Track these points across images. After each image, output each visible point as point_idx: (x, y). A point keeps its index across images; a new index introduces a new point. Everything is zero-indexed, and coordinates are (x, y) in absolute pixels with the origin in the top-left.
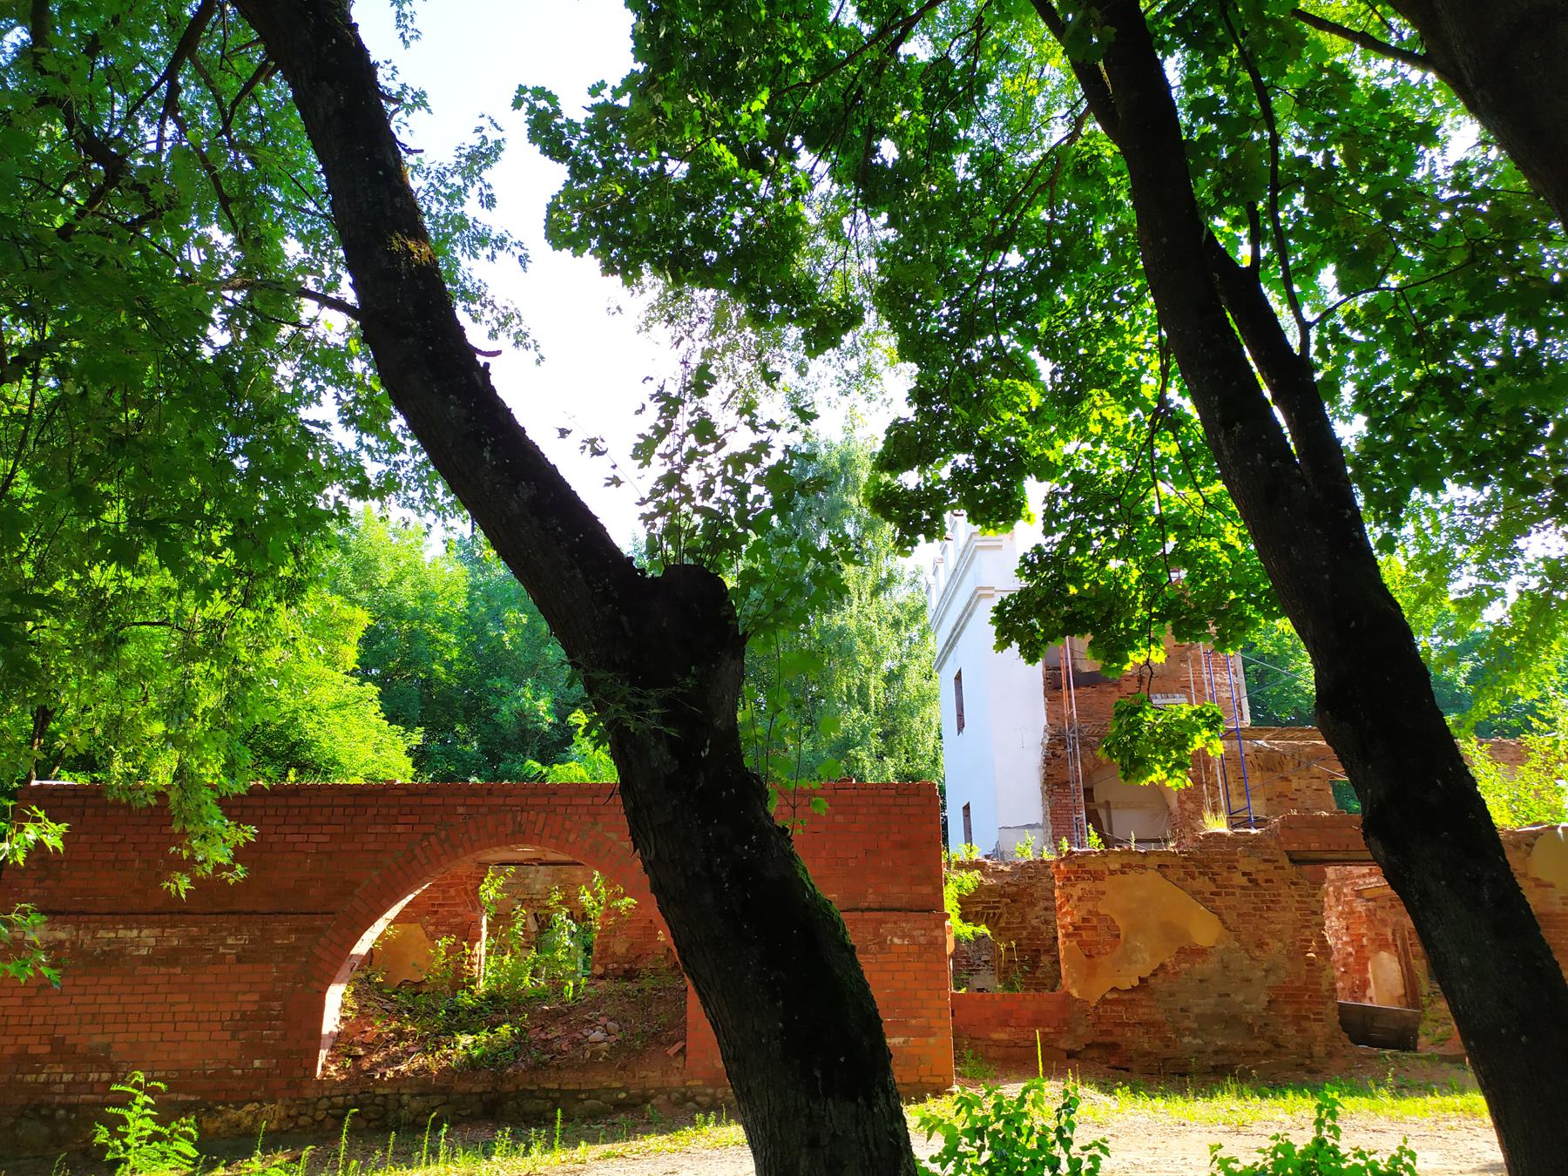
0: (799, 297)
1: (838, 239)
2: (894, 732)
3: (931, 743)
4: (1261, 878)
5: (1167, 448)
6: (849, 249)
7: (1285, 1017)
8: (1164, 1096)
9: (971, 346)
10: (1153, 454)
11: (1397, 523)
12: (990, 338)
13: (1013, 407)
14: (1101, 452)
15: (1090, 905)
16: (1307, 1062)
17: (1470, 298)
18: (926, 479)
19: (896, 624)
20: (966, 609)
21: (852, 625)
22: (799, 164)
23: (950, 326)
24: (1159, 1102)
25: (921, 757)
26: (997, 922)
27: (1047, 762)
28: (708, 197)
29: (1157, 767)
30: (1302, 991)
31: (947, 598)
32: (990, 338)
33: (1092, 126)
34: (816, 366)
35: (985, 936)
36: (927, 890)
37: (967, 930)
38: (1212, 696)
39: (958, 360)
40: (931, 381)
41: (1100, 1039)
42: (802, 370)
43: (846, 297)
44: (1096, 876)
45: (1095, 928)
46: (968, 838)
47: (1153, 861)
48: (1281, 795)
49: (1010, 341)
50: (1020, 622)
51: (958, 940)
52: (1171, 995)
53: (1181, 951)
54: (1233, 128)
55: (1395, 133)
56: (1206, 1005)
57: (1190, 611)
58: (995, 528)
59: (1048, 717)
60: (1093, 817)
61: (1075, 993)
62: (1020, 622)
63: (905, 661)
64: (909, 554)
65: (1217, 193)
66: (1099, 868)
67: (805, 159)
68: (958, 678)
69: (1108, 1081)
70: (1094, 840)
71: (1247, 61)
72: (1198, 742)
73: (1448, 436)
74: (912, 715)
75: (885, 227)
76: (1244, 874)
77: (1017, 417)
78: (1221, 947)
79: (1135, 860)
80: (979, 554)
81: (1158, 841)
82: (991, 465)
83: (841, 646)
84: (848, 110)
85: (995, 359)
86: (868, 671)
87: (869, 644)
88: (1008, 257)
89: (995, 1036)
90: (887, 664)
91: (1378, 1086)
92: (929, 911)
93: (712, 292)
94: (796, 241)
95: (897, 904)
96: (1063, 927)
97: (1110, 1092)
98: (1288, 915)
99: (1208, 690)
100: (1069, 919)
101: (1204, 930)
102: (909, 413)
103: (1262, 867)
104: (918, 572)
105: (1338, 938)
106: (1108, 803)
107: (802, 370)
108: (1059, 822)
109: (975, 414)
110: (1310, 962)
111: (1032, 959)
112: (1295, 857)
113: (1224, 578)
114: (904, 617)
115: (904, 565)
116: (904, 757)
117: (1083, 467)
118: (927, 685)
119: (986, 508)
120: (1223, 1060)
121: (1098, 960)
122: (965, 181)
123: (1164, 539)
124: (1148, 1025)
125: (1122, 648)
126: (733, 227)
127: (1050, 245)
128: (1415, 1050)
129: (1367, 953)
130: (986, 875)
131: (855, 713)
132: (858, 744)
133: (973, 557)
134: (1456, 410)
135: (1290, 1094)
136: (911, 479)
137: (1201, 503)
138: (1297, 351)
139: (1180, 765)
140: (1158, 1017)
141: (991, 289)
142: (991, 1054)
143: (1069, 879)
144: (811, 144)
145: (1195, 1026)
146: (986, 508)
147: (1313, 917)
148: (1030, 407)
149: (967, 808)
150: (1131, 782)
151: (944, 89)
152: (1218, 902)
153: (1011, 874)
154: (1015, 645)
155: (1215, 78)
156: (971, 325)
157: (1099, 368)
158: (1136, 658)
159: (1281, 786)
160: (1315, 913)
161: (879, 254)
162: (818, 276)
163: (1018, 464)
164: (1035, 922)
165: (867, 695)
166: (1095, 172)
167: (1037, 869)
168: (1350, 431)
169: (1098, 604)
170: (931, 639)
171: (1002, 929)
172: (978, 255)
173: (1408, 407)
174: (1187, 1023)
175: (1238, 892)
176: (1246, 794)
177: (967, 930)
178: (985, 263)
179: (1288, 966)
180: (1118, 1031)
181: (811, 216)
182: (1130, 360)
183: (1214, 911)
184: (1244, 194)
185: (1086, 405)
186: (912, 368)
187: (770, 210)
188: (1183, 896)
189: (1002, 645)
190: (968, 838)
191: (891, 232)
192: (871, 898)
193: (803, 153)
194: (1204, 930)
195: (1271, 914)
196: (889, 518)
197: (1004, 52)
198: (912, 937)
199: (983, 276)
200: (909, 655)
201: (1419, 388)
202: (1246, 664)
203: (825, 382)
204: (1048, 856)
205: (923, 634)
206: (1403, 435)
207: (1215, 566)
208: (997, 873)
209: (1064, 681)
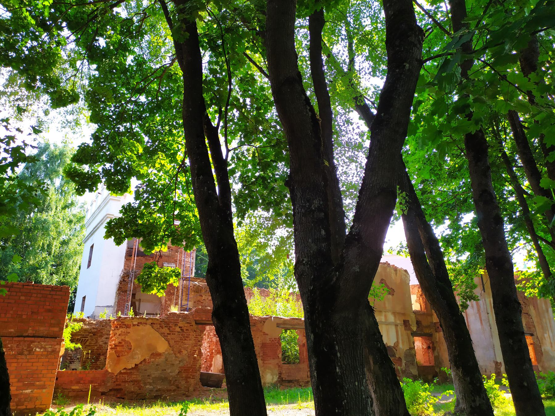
0: (52, 84)
1: (73, 68)
2: (60, 264)
3: (75, 270)
4: (185, 329)
5: (182, 178)
6: (81, 74)
7: (182, 377)
8: (134, 408)
9: (120, 124)
10: (177, 180)
11: (243, 218)
12: (128, 124)
13: (132, 151)
14: (160, 175)
15: (123, 337)
16: (187, 393)
17: (275, 156)
18: (92, 170)
19: (70, 222)
20: (101, 221)
21: (51, 219)
22: (62, 33)
23: (114, 115)
24: (132, 410)
25: (70, 276)
26: (86, 343)
27: (121, 282)
28: (16, 32)
29: (155, 288)
30: (190, 368)
31: (94, 216)
32: (128, 124)
33: (176, 63)
34: (54, 113)
35: (80, 348)
36: (56, 329)
37: (72, 346)
38: (184, 265)
39: (114, 128)
40: (102, 134)
41: (116, 387)
42: (46, 113)
43: (72, 90)
44: (128, 327)
45: (123, 346)
46: (82, 310)
47: (150, 322)
48: (199, 301)
49: (136, 127)
50: (116, 230)
51: (67, 350)
52: (145, 370)
53: (153, 354)
54: (220, 82)
55: (264, 100)
56: (156, 374)
57: (178, 236)
58: (116, 193)
59: (125, 266)
60: (133, 304)
61: (110, 370)
62: (116, 230)
63: (71, 237)
64: (81, 195)
65: (211, 100)
66: (129, 323)
67: (66, 32)
68: (92, 247)
69: (115, 403)
70: (131, 314)
71: (227, 62)
72: (172, 280)
73: (262, 195)
74: (69, 258)
75: (95, 70)
76: (180, 327)
77: (133, 155)
78: (166, 353)
79: (143, 321)
80: (111, 201)
81: (154, 314)
82: (120, 170)
83: (44, 227)
84: (88, 21)
85: (129, 132)
86: (54, 239)
87: (57, 228)
88: (141, 97)
89: (74, 387)
90: (63, 237)
91: (207, 400)
92: (56, 338)
93: (10, 69)
94: (54, 63)
95: (41, 335)
96: (111, 345)
97: (114, 407)
98: (191, 342)
99: (183, 263)
100: (113, 342)
101: (162, 347)
102: (90, 142)
103: (186, 325)
104: (84, 204)
105: (206, 350)
106: (140, 299)
107: (46, 113)
108: (120, 305)
109: (117, 150)
110: (195, 358)
111: (96, 358)
112: (197, 322)
113: (191, 226)
114: (75, 220)
115: (79, 200)
116: (62, 275)
117: (153, 179)
118: (78, 248)
119: (114, 185)
120: (159, 393)
121: (121, 358)
122: (130, 65)
123: (175, 209)
124: (135, 382)
125: (152, 244)
126: (26, 47)
127: (157, 98)
128: (221, 387)
129: (213, 355)
130: (85, 324)
131: (44, 255)
132: (43, 268)
133: (108, 202)
134: (265, 188)
135: (178, 405)
136: (86, 168)
137: (189, 200)
138: (224, 158)
139: (163, 288)
140: (140, 378)
141: (132, 107)
142: (70, 395)
143: (117, 327)
144: (70, 27)
145: (152, 381)
146: (114, 185)
147: (198, 343)
148: (138, 153)
149: (84, 298)
150: (145, 293)
151: (128, 30)
152: (169, 337)
153: (95, 324)
154: (113, 238)
155: (217, 63)
156: (122, 117)
157: (164, 145)
158: (157, 249)
159: (199, 298)
160: (199, 341)
161: (90, 79)
162: (62, 79)
163: (130, 172)
164: (101, 343)
165: (51, 249)
166: (175, 79)
167: (106, 323)
168: (236, 187)
169: (147, 228)
170: (84, 230)
171: (87, 345)
172: (129, 93)
173: (253, 183)
174: (149, 380)
175: (176, 333)
176: (187, 300)
177: (72, 346)
178: (131, 97)
179: (187, 360)
180: (123, 384)
181: (63, 55)
182: (175, 146)
183: (167, 340)
184: (219, 103)
185: (156, 156)
186: (94, 127)
187: (46, 46)
188: (157, 334)
189: (108, 236)
190: (82, 310)
191: (97, 72)
192: (30, 332)
193: (66, 29)
194: (162, 347)
195: (186, 341)
196: (74, 181)
197: (153, 26)
198: (45, 348)
199: (130, 101)
200: (73, 235)
201: (257, 178)
202: (197, 256)
203: (56, 121)
204: (112, 318)
205: (82, 227)
206: (251, 191)
207: (190, 222)
208: (90, 324)
209: (133, 254)
